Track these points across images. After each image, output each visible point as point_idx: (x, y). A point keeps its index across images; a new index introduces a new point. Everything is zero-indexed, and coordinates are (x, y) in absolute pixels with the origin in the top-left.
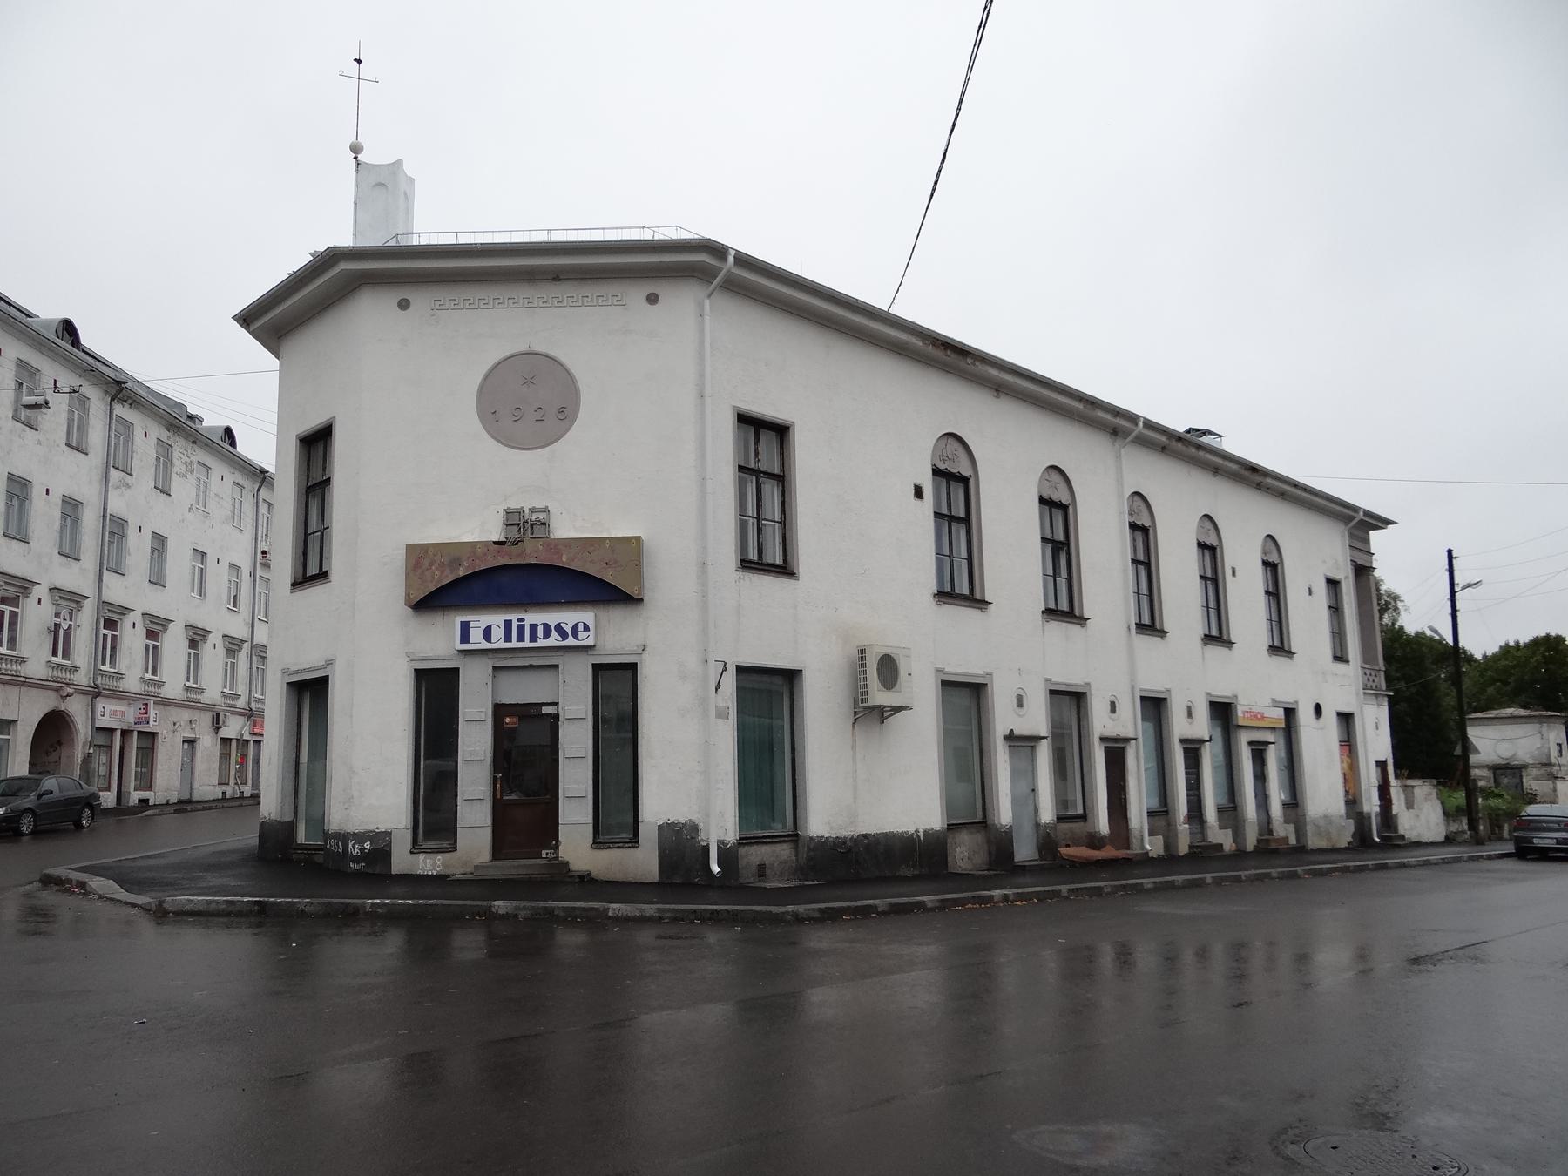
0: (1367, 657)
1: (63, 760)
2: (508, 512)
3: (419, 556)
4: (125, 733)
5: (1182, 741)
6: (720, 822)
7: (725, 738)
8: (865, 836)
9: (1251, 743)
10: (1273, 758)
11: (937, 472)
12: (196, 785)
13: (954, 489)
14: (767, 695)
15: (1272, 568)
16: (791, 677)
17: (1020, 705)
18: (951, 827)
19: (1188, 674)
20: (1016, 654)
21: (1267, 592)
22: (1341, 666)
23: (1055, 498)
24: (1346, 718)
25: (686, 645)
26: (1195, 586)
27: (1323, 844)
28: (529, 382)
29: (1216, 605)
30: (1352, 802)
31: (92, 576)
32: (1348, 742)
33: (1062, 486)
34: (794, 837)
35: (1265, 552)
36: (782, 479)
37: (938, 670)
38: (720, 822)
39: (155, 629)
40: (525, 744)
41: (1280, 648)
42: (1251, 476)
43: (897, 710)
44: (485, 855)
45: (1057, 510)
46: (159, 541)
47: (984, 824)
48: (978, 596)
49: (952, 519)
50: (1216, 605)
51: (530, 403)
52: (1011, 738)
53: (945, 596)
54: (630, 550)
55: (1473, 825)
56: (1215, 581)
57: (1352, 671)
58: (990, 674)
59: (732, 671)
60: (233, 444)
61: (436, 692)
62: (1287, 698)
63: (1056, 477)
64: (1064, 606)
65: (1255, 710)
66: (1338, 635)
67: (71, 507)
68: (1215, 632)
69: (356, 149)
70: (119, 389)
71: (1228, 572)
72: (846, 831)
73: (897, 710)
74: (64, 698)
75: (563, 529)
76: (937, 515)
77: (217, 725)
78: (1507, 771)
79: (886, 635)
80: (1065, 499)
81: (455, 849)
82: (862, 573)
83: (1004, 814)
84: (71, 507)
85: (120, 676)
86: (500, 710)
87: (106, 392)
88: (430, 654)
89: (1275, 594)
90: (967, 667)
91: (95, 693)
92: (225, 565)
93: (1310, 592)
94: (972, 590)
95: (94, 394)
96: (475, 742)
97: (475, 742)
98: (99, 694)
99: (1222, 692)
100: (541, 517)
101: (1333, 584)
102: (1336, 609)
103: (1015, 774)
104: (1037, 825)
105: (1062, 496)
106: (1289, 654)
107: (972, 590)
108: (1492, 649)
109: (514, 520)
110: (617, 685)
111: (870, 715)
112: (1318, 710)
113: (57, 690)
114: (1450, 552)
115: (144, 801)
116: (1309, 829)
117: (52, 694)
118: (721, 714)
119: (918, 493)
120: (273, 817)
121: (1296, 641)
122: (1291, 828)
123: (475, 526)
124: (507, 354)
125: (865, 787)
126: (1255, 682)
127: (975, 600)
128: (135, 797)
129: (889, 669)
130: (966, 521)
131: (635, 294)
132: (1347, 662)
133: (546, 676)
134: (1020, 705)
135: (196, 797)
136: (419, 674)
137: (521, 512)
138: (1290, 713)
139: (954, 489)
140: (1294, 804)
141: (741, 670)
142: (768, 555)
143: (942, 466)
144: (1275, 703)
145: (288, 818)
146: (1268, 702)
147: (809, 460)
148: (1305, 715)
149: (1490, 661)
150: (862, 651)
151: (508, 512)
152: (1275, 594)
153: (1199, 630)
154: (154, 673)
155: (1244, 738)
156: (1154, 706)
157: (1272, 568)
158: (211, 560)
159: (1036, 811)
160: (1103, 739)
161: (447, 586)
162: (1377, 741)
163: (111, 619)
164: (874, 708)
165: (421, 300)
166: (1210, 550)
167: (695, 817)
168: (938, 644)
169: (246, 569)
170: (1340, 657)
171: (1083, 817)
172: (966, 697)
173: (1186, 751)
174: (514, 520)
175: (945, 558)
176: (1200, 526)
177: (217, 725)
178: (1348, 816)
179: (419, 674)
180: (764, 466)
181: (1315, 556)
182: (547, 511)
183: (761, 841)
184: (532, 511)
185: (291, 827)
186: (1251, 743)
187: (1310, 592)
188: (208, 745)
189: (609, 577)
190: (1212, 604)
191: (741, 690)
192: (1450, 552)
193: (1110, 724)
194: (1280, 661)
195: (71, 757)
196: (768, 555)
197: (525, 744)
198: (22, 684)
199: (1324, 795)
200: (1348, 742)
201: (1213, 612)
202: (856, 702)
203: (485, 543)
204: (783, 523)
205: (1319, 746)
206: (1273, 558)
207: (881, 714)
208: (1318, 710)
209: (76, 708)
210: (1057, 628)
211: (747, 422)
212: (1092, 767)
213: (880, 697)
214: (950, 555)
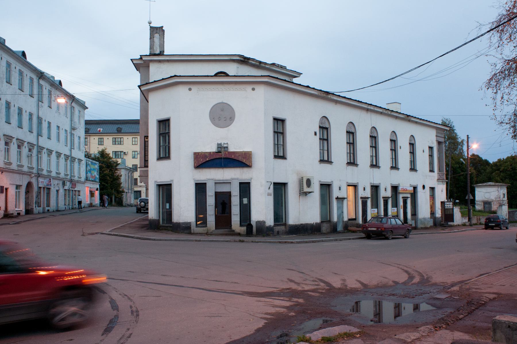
0: (440, 170)
1: (30, 197)
2: (218, 144)
3: (197, 155)
4: (44, 188)
5: (383, 198)
6: (270, 221)
7: (271, 199)
8: (302, 224)
9: (403, 198)
10: (409, 201)
11: (320, 127)
12: (59, 205)
13: (324, 131)
14: (279, 189)
15: (412, 145)
16: (284, 185)
17: (340, 189)
18: (322, 222)
19: (385, 178)
20: (338, 174)
21: (410, 152)
22: (432, 174)
23: (351, 131)
24: (432, 189)
25: (260, 178)
26: (389, 152)
27: (423, 226)
28: (222, 110)
29: (395, 158)
30: (433, 213)
31: (35, 138)
32: (433, 197)
33: (353, 127)
34: (285, 224)
35: (410, 140)
36: (283, 133)
37: (320, 181)
38: (270, 221)
39: (50, 152)
40: (223, 201)
41: (413, 169)
42: (408, 118)
43: (310, 192)
44: (214, 228)
45: (351, 134)
46: (49, 123)
47: (330, 221)
48: (330, 160)
49: (324, 139)
50: (395, 158)
51: (222, 116)
52: (337, 198)
53: (322, 161)
54: (248, 155)
55: (469, 219)
56: (395, 150)
57: (435, 175)
58: (332, 182)
59: (272, 184)
60: (61, 85)
61: (201, 188)
62: (414, 184)
63: (351, 125)
64: (352, 161)
65: (405, 188)
66: (431, 163)
67: (31, 115)
68: (394, 166)
69: (150, 23)
70: (41, 75)
71: (399, 148)
72: (297, 223)
73: (310, 192)
74: (32, 178)
75: (231, 149)
76: (320, 139)
77: (64, 184)
78: (487, 203)
79: (308, 174)
80: (353, 131)
81: (206, 226)
82: (302, 159)
83: (335, 219)
84: (31, 115)
85: (42, 170)
86: (216, 193)
87: (37, 76)
88: (199, 179)
89: (413, 153)
90: (326, 180)
91: (39, 175)
92: (64, 130)
93: (423, 151)
94: (328, 159)
95: (34, 77)
96: (211, 201)
97: (211, 201)
98: (39, 176)
99: (395, 183)
100: (225, 146)
101: (431, 148)
102: (431, 156)
103: (338, 209)
104: (343, 221)
105: (352, 130)
106: (416, 171)
107: (328, 159)
108: (496, 160)
109: (219, 146)
110: (245, 188)
111: (304, 194)
112: (424, 187)
113: (30, 175)
114: (468, 136)
115: (48, 210)
116: (419, 222)
117: (28, 176)
118: (269, 195)
119: (315, 134)
120: (154, 218)
121: (418, 166)
122: (414, 222)
123: (210, 148)
124: (216, 103)
125: (304, 211)
126: (405, 179)
127: (329, 162)
128: (47, 208)
129: (309, 183)
130: (327, 140)
131: (249, 88)
132: (434, 172)
133: (228, 185)
134: (340, 189)
135: (59, 209)
136: (196, 184)
137: (221, 144)
138: (415, 188)
139: (324, 131)
140: (414, 214)
141: (274, 183)
142: (280, 156)
143: (321, 126)
144: (411, 186)
145: (158, 219)
146: (409, 185)
147: (290, 128)
148: (420, 189)
149: (495, 164)
150: (302, 178)
151: (218, 144)
152: (413, 153)
153: (390, 165)
154: (20, 162)
155: (401, 196)
156: (375, 188)
157: (412, 145)
158: (61, 128)
159: (343, 217)
160: (361, 198)
161: (204, 162)
162: (441, 194)
163: (40, 149)
164: (305, 192)
165: (194, 88)
166: (393, 142)
167: (264, 220)
168: (320, 174)
169: (69, 131)
170: (432, 171)
171: (355, 219)
172: (326, 188)
173: (384, 200)
174: (219, 146)
175: (322, 150)
176: (391, 135)
177: (64, 184)
178: (431, 218)
179: (196, 184)
180: (279, 131)
181: (427, 139)
182: (227, 144)
183: (278, 225)
184: (224, 144)
185: (159, 220)
186: (403, 198)
187: (423, 151)
188: (61, 191)
189: (244, 161)
190: (394, 157)
191: (274, 188)
192: (468, 136)
193: (363, 194)
194: (413, 173)
195: (32, 196)
196: (280, 156)
197: (223, 201)
198: (23, 174)
199: (424, 211)
200: (433, 197)
201: (394, 160)
202: (300, 191)
203: (213, 152)
204: (283, 145)
205: (423, 198)
206: (413, 142)
207: (306, 194)
208: (424, 187)
209: (34, 181)
210: (350, 168)
211: (276, 119)
212: (358, 206)
213: (306, 189)
214: (323, 150)
